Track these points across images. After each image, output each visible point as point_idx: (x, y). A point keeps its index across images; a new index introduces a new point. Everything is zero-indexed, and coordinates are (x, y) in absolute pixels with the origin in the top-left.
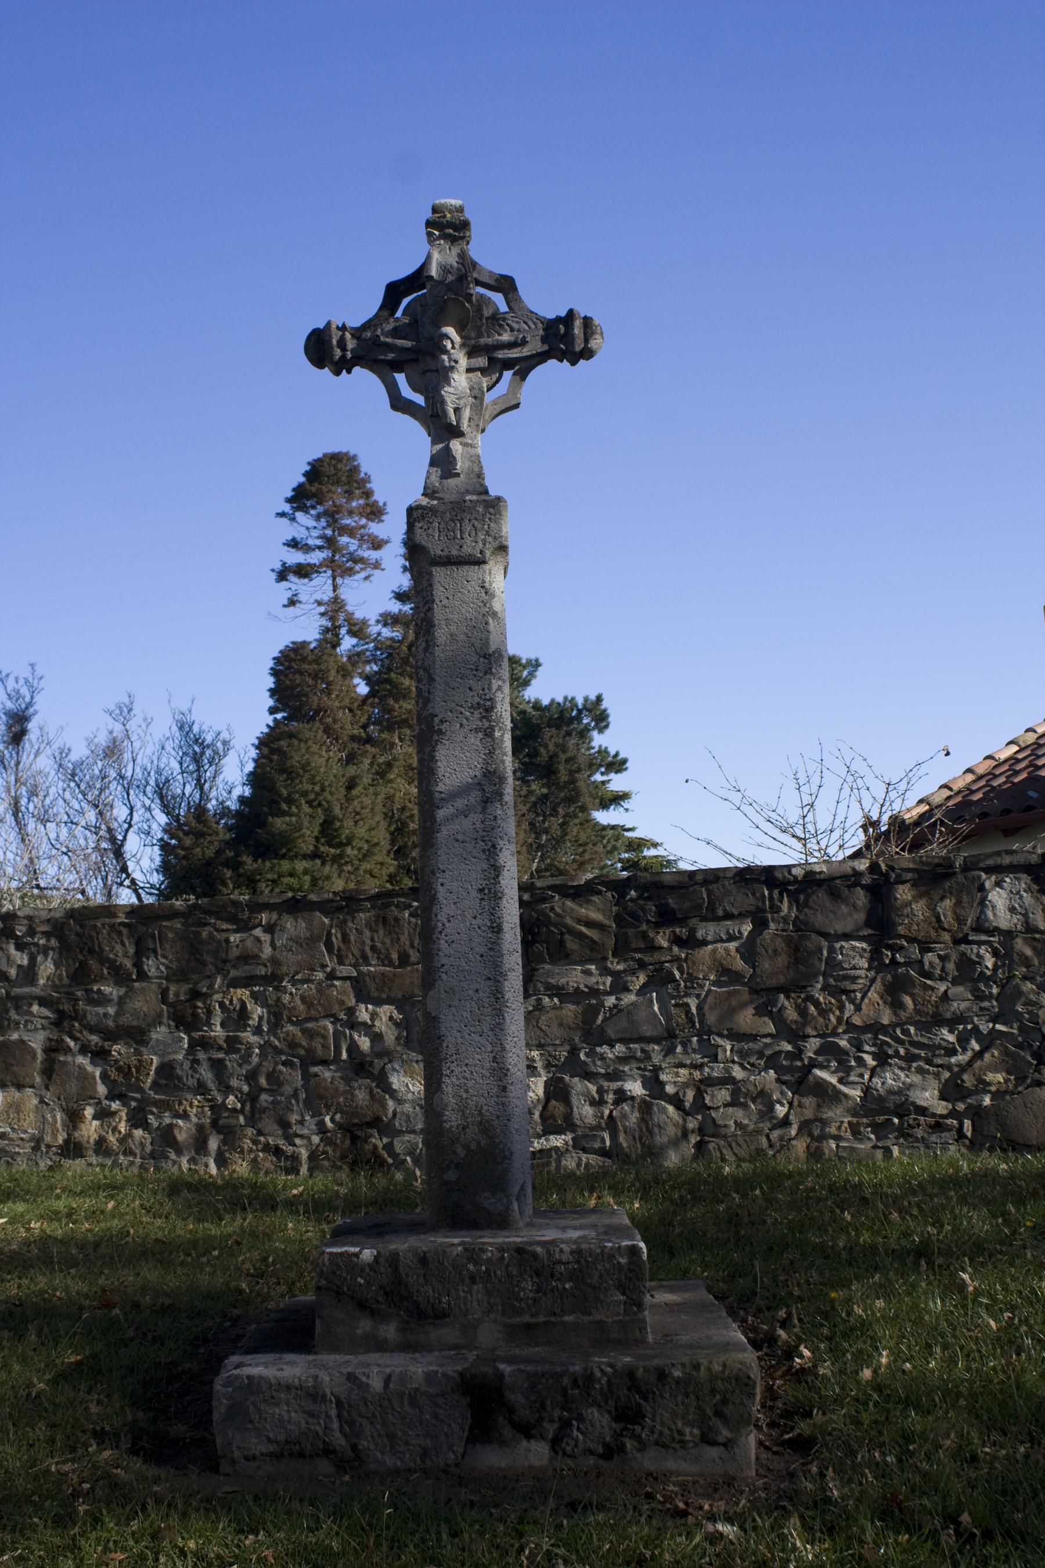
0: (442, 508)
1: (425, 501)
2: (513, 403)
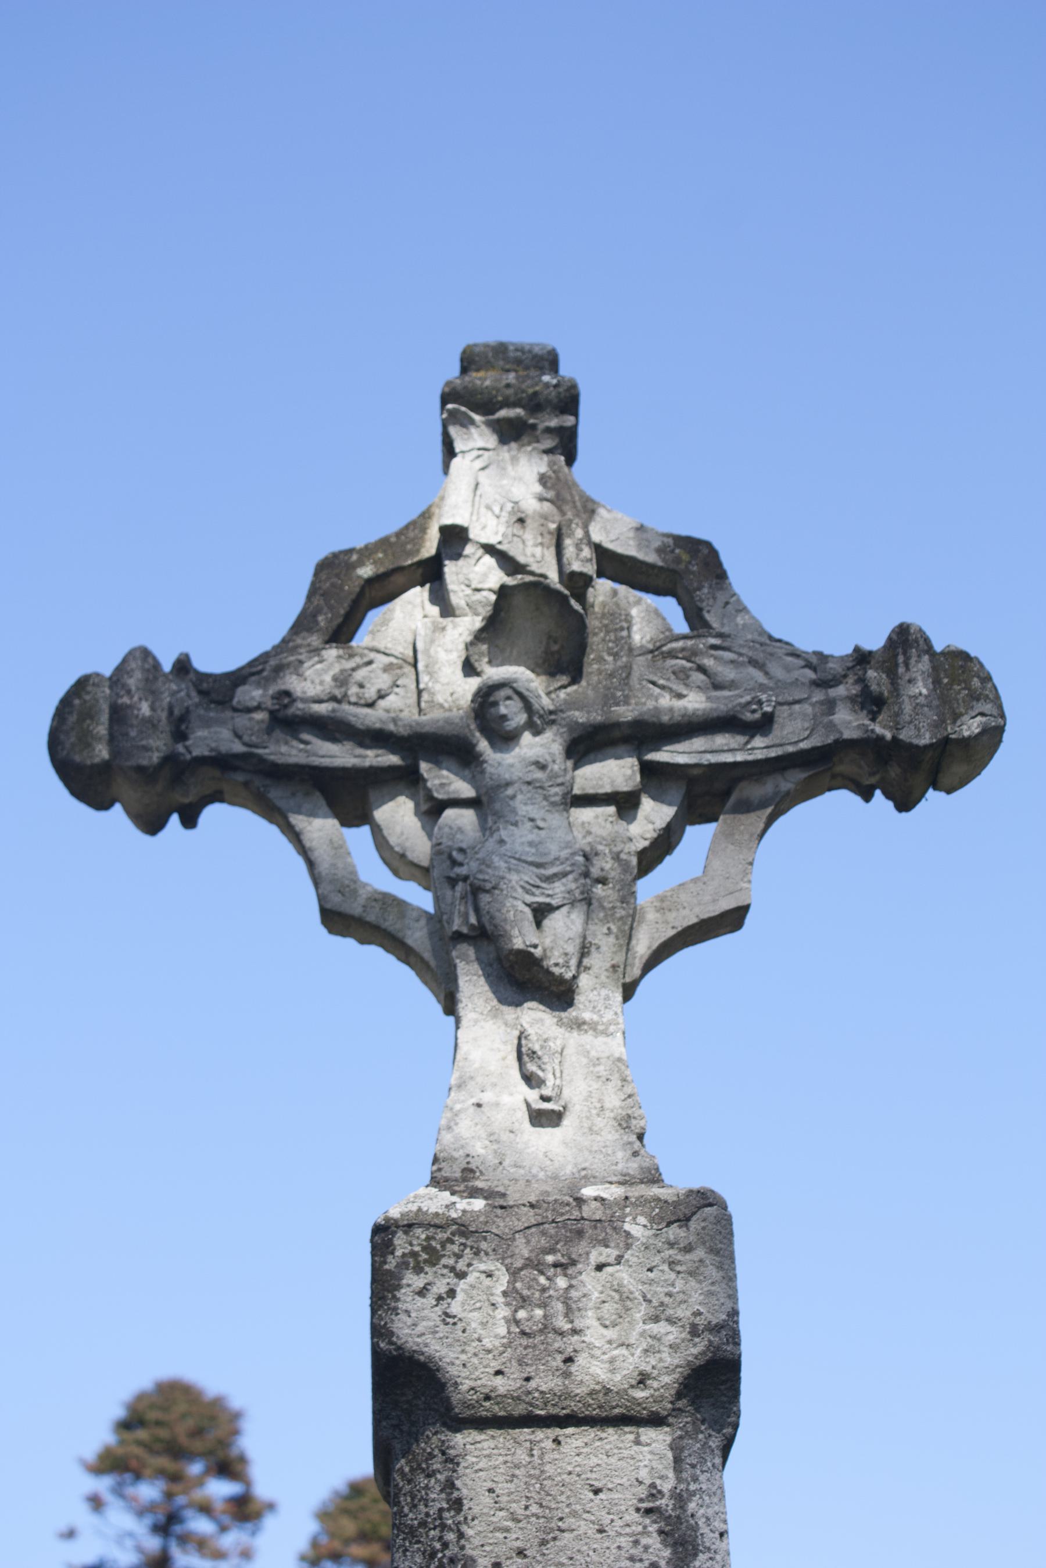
0: (502, 1225)
1: (437, 1202)
2: (727, 904)
